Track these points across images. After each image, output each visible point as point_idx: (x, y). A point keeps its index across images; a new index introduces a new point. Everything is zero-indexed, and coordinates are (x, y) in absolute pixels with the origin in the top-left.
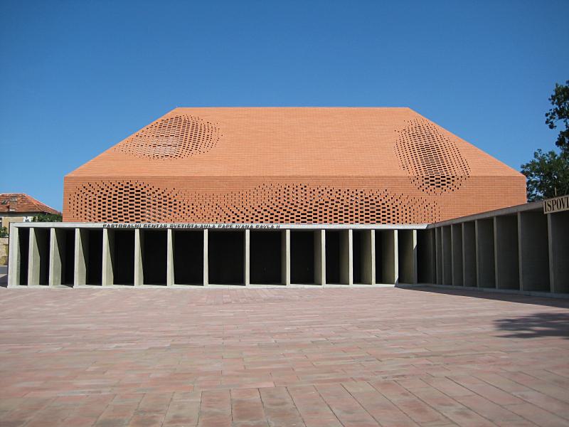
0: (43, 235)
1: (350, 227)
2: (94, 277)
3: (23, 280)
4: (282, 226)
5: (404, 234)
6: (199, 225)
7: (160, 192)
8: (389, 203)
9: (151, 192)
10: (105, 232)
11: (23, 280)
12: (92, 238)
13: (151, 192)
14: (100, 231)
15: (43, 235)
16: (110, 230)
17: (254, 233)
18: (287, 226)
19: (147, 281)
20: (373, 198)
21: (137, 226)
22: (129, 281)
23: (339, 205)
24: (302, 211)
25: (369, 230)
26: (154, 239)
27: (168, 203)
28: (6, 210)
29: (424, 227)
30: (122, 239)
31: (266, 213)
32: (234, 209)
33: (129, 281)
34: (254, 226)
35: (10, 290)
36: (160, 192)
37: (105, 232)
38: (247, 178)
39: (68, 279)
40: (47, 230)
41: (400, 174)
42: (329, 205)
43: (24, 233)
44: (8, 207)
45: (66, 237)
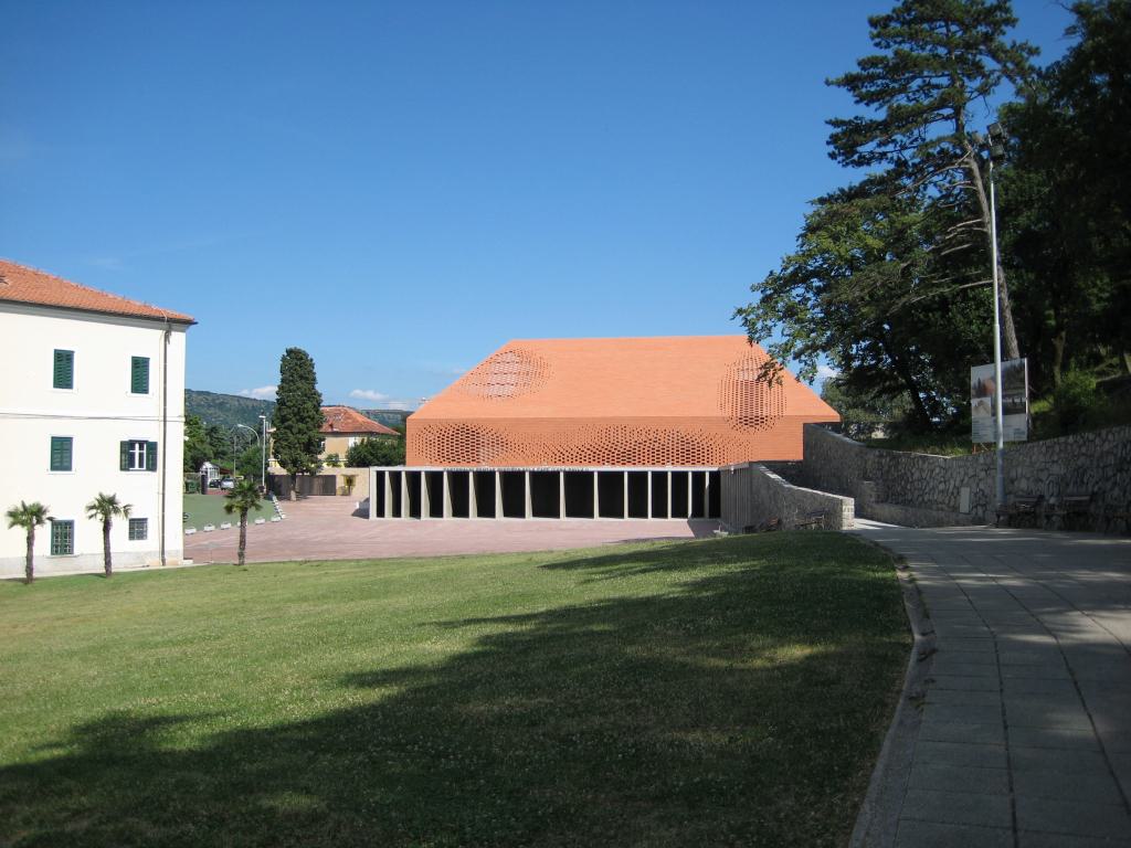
0: (396, 477)
1: (626, 469)
2: (436, 511)
3: (381, 513)
4: (590, 469)
5: (699, 476)
6: (521, 469)
7: (493, 432)
8: (704, 442)
9: (484, 433)
10: (445, 474)
11: (381, 513)
12: (435, 479)
13: (484, 433)
14: (441, 473)
15: (396, 477)
16: (449, 472)
17: (568, 475)
18: (595, 468)
19: (507, 513)
20: (688, 437)
21: (471, 468)
22: (492, 514)
23: (657, 445)
24: (622, 450)
25: (622, 473)
26: (485, 479)
27: (500, 443)
28: (330, 430)
29: (715, 469)
30: (459, 479)
31: (589, 452)
32: (559, 448)
33: (492, 514)
34: (567, 469)
35: (372, 522)
36: (493, 432)
37: (445, 474)
38: (571, 420)
39: (397, 513)
40: (399, 473)
41: (715, 414)
42: (647, 444)
43: (380, 476)
44: (331, 426)
45: (414, 478)
